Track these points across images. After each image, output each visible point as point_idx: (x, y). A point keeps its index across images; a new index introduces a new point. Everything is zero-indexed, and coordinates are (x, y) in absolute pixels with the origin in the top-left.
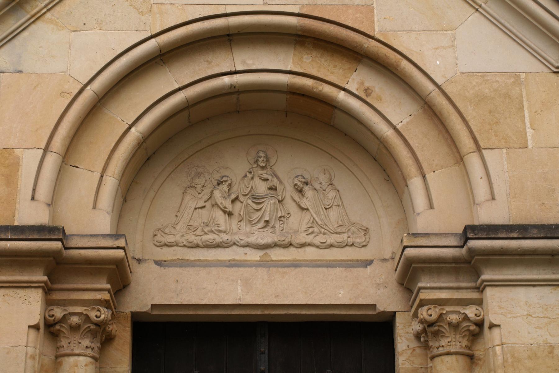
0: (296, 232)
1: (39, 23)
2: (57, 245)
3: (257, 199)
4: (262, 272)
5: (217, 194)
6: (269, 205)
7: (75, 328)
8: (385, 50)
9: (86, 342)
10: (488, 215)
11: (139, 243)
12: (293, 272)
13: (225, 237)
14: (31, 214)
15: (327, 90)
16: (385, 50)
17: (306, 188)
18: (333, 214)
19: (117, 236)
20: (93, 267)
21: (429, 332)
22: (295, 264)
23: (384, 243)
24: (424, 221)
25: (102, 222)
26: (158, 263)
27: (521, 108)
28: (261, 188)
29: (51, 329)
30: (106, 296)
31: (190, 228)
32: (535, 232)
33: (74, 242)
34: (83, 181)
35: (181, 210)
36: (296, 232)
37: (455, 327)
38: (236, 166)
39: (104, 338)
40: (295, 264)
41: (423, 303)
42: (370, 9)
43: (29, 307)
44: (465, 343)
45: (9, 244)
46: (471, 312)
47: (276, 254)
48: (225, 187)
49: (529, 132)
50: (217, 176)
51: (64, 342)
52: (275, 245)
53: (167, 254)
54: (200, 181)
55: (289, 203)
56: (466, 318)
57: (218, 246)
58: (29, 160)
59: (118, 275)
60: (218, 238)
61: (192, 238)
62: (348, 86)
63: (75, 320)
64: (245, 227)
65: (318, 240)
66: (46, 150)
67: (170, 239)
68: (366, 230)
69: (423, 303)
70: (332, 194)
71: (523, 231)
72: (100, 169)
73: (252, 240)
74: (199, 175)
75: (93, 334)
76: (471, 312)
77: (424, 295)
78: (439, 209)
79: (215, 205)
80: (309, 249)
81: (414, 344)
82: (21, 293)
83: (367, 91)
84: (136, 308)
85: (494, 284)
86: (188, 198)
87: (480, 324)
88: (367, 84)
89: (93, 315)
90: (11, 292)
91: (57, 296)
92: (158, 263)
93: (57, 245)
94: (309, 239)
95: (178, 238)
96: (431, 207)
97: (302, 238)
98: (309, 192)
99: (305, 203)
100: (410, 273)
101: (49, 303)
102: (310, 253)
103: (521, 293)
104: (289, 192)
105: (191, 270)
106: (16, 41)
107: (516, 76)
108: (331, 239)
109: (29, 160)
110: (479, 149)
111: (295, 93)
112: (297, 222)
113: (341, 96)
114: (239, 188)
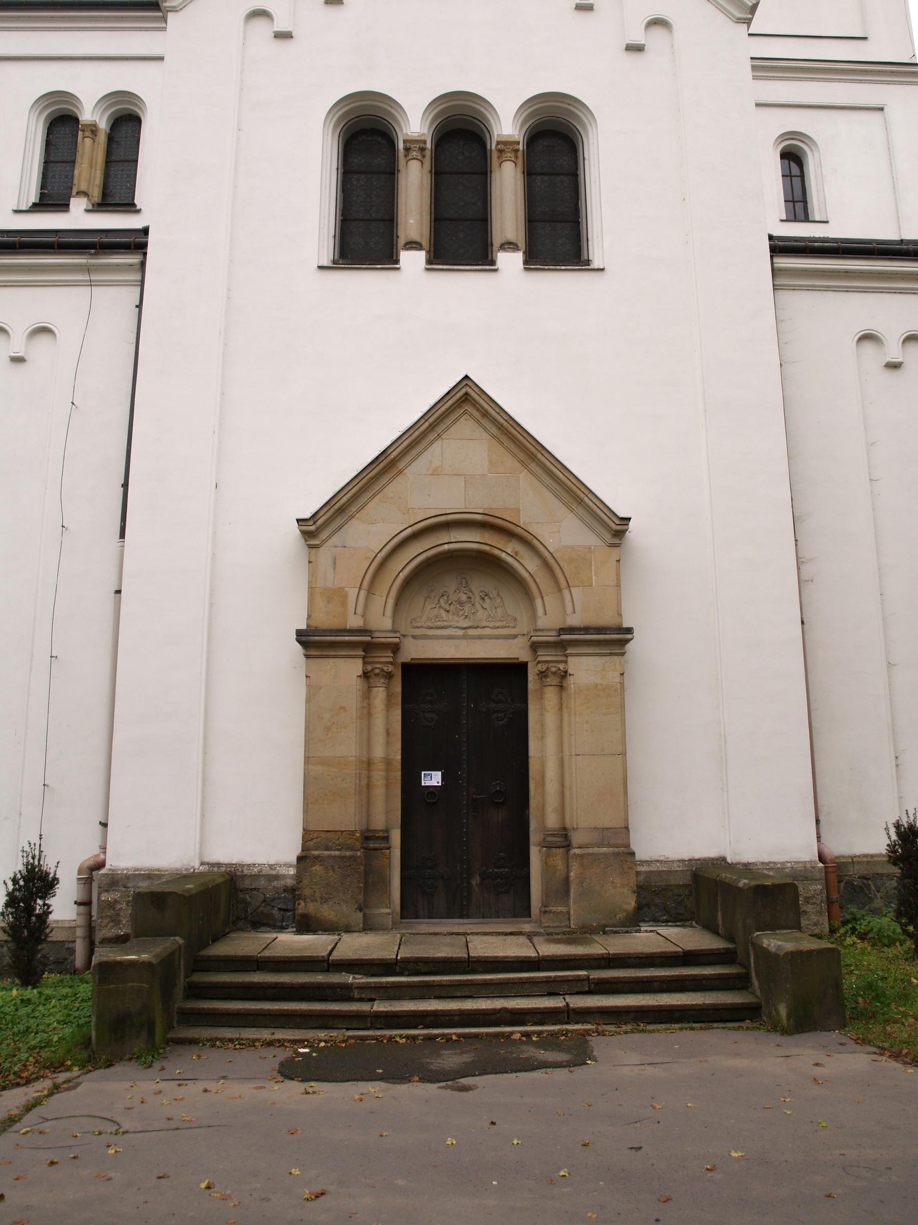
0: (481, 620)
1: (353, 520)
2: (369, 638)
3: (461, 603)
4: (464, 642)
5: (442, 601)
6: (467, 607)
7: (377, 675)
8: (526, 534)
9: (382, 681)
10: (574, 620)
11: (404, 628)
12: (478, 641)
13: (446, 624)
14: (354, 622)
15: (497, 552)
16: (526, 534)
17: (486, 598)
18: (499, 611)
19: (396, 632)
20: (385, 646)
21: (543, 675)
22: (480, 637)
23: (524, 626)
24: (543, 622)
25: (387, 623)
26: (414, 637)
27: (591, 565)
28: (464, 598)
29: (366, 675)
30: (391, 660)
31: (429, 619)
32: (592, 631)
33: (376, 635)
34: (378, 601)
35: (425, 610)
36: (481, 620)
37: (554, 673)
38: (451, 585)
39: (389, 676)
40: (480, 637)
41: (539, 662)
42: (518, 511)
43: (356, 667)
44: (559, 680)
45: (347, 638)
46: (561, 666)
47: (471, 632)
48: (445, 597)
49: (594, 577)
50: (442, 591)
51: (372, 681)
52: (470, 627)
53: (418, 632)
54: (433, 594)
55: (478, 606)
56: (559, 669)
57: (442, 628)
58: (352, 593)
59: (395, 648)
60: (442, 624)
61: (430, 624)
62: (506, 550)
63: (377, 671)
64: (455, 618)
65: (492, 624)
66: (360, 588)
67: (419, 624)
68: (515, 619)
69: (539, 662)
70: (498, 601)
71: (586, 630)
72: (385, 595)
73: (459, 625)
74: (432, 591)
75: (385, 677)
76: (561, 666)
77: (540, 659)
78: (550, 616)
79: (441, 607)
80: (487, 629)
81: (536, 677)
82: (352, 660)
83: (516, 553)
84: (404, 660)
85: (572, 655)
86: (427, 603)
87: (566, 672)
88: (516, 549)
89: (385, 668)
90: (348, 660)
91: (368, 660)
92: (414, 637)
93: (369, 638)
94: (487, 624)
95: (423, 624)
96: (546, 614)
97: (484, 624)
98: (487, 600)
99: (485, 606)
100: (535, 647)
101: (365, 663)
102: (488, 631)
103: (584, 659)
104: (477, 600)
105: (430, 641)
106: (342, 530)
107: (590, 548)
108: (498, 624)
109: (352, 593)
110: (569, 587)
111: (480, 553)
112: (481, 614)
113: (503, 555)
114: (454, 598)
